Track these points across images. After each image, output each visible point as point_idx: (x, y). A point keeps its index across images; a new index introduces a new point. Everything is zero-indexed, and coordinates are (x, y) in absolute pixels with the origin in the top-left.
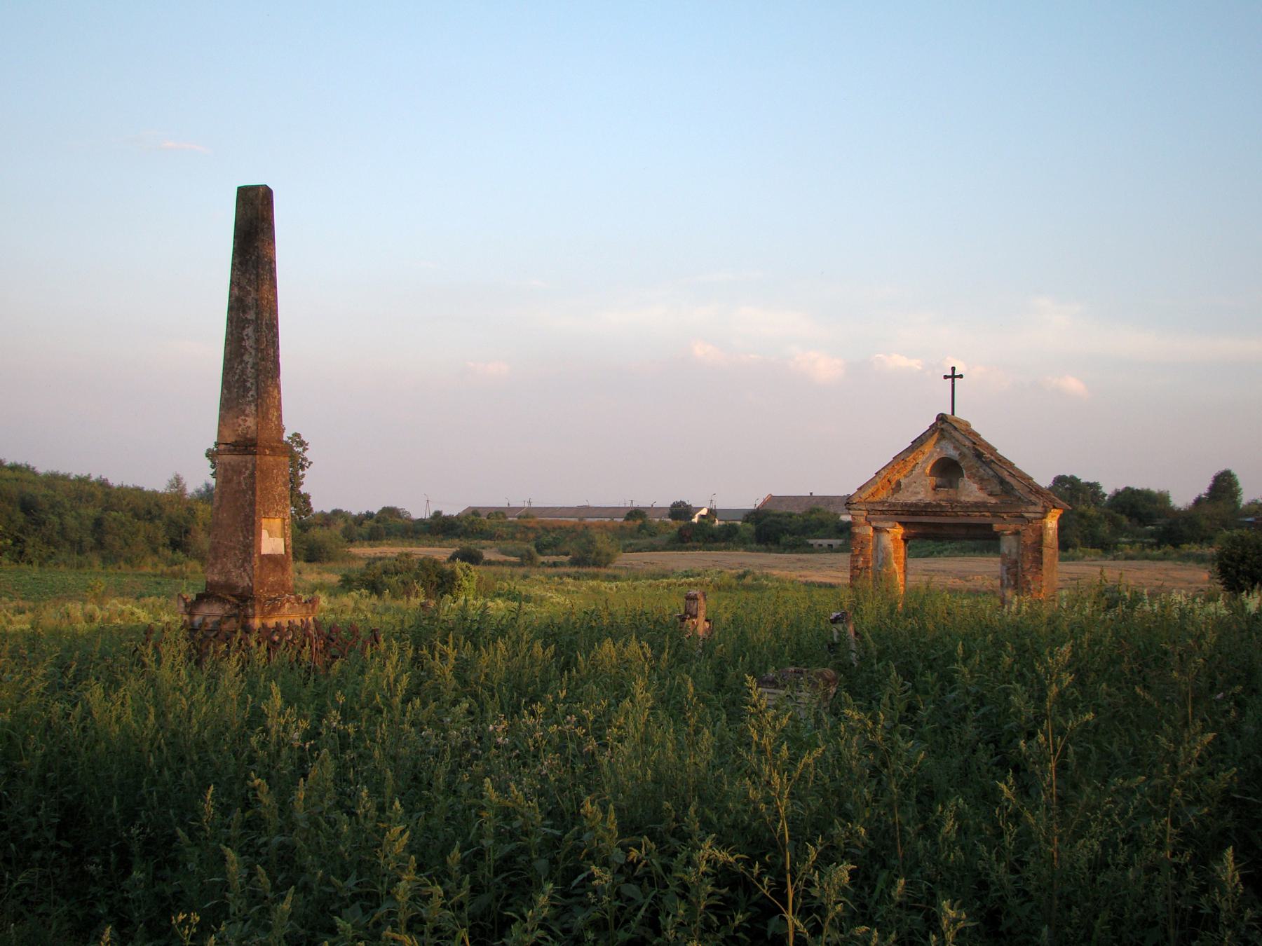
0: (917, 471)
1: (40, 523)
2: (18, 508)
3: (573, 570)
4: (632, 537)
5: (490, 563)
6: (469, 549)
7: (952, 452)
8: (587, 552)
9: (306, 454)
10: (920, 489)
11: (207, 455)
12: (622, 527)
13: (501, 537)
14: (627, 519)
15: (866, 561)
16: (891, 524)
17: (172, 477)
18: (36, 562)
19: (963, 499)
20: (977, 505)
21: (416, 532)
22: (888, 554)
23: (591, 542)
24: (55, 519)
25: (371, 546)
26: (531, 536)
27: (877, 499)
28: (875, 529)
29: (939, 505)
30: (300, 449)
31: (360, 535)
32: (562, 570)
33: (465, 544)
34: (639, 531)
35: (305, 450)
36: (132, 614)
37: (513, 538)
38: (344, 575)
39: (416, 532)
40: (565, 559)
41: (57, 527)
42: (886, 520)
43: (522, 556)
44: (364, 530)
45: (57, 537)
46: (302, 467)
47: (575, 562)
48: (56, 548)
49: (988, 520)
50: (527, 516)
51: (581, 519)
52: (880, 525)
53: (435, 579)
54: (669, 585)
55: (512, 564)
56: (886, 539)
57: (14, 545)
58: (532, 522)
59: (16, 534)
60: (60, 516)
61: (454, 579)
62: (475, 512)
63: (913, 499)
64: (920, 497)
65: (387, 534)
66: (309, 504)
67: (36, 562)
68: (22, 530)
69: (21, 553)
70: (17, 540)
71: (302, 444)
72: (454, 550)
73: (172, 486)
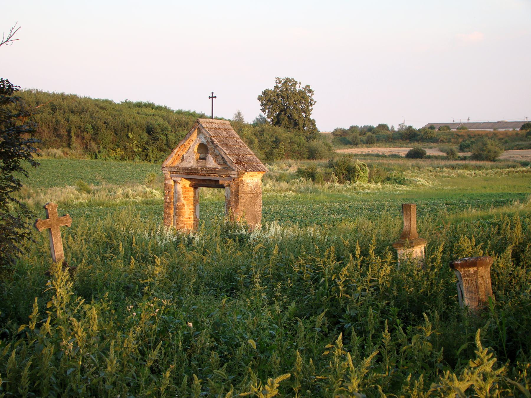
0: (191, 150)
1: (156, 139)
2: (145, 132)
3: (474, 163)
4: (522, 140)
5: (429, 157)
6: (418, 149)
7: (204, 141)
8: (483, 151)
9: (313, 97)
10: (192, 160)
11: (259, 99)
12: (517, 134)
13: (442, 141)
14: (522, 129)
15: (170, 199)
16: (179, 179)
17: (236, 112)
18: (153, 161)
19: (208, 166)
20: (213, 170)
21: (394, 139)
22: (179, 195)
23: (485, 145)
24: (164, 138)
25: (368, 147)
26: (460, 140)
27: (175, 165)
28: (174, 181)
29: (197, 170)
30: (310, 94)
31: (362, 141)
32: (467, 162)
33: (417, 145)
34: (526, 136)
35: (312, 95)
36: (152, 193)
37: (449, 141)
38: (298, 169)
39: (394, 139)
40: (469, 154)
41: (165, 141)
42: (178, 177)
43: (448, 153)
44: (364, 138)
45: (165, 147)
46: (311, 105)
47: (476, 157)
48: (164, 152)
49: (217, 178)
50: (462, 128)
51: (495, 129)
52: (176, 179)
53: (344, 171)
54: (509, 172)
55: (443, 158)
56: (179, 187)
57: (143, 151)
58: (463, 132)
59: (144, 145)
60: (166, 135)
61: (354, 171)
62: (431, 127)
63: (188, 166)
64: (191, 164)
65: (378, 140)
66: (315, 125)
67: (153, 161)
68: (147, 143)
69: (147, 155)
70: (144, 149)
71: (311, 91)
72: (409, 149)
73: (236, 117)
